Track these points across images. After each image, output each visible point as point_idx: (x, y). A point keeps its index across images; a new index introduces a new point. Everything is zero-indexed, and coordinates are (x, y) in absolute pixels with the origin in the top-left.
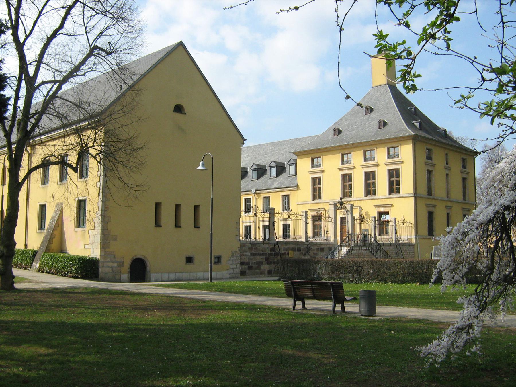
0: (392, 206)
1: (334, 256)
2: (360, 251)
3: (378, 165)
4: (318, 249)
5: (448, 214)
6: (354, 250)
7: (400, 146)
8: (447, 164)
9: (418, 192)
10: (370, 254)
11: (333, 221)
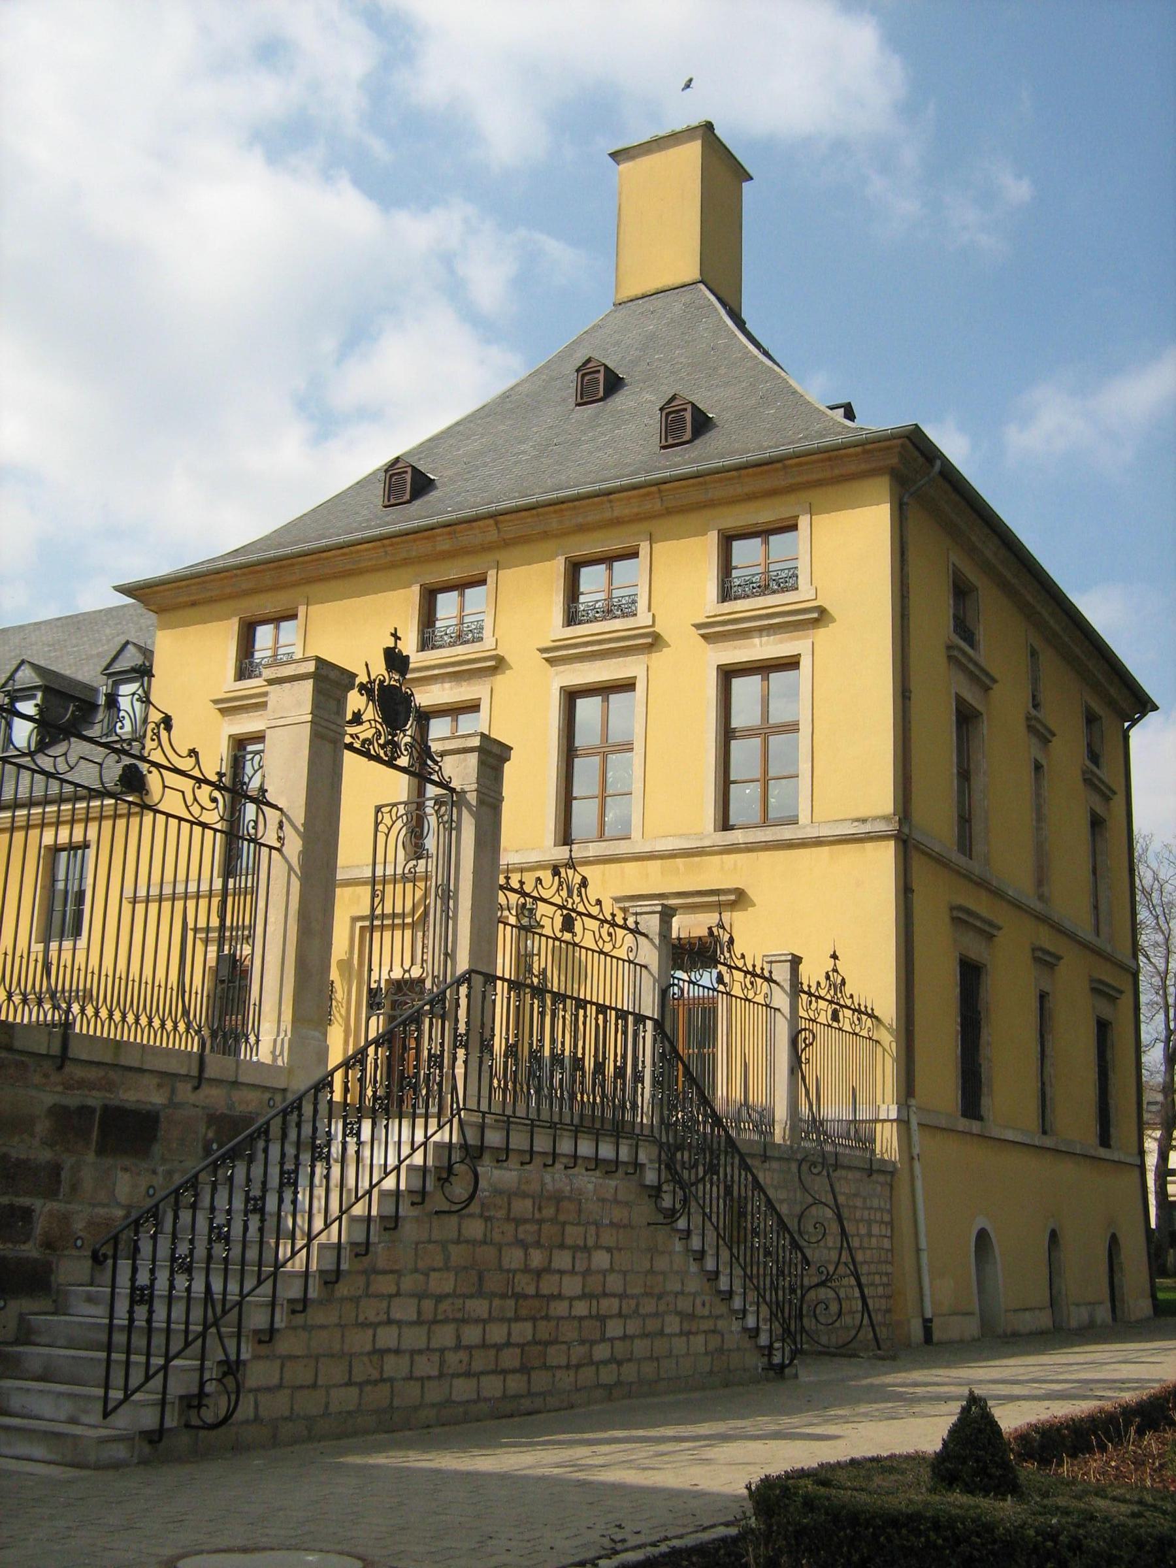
0: (739, 899)
1: (256, 1206)
2: (556, 1179)
3: (653, 642)
4: (69, 1123)
5: (1043, 997)
6: (503, 1155)
7: (803, 522)
8: (1036, 706)
9: (916, 817)
10: (643, 1211)
11: (294, 846)
